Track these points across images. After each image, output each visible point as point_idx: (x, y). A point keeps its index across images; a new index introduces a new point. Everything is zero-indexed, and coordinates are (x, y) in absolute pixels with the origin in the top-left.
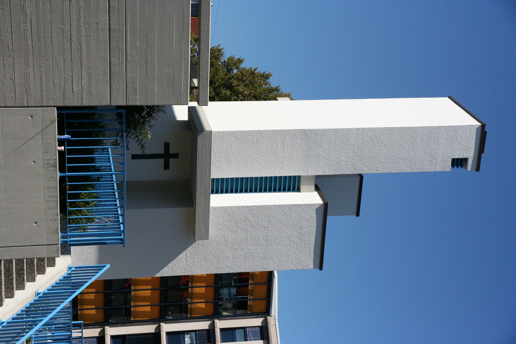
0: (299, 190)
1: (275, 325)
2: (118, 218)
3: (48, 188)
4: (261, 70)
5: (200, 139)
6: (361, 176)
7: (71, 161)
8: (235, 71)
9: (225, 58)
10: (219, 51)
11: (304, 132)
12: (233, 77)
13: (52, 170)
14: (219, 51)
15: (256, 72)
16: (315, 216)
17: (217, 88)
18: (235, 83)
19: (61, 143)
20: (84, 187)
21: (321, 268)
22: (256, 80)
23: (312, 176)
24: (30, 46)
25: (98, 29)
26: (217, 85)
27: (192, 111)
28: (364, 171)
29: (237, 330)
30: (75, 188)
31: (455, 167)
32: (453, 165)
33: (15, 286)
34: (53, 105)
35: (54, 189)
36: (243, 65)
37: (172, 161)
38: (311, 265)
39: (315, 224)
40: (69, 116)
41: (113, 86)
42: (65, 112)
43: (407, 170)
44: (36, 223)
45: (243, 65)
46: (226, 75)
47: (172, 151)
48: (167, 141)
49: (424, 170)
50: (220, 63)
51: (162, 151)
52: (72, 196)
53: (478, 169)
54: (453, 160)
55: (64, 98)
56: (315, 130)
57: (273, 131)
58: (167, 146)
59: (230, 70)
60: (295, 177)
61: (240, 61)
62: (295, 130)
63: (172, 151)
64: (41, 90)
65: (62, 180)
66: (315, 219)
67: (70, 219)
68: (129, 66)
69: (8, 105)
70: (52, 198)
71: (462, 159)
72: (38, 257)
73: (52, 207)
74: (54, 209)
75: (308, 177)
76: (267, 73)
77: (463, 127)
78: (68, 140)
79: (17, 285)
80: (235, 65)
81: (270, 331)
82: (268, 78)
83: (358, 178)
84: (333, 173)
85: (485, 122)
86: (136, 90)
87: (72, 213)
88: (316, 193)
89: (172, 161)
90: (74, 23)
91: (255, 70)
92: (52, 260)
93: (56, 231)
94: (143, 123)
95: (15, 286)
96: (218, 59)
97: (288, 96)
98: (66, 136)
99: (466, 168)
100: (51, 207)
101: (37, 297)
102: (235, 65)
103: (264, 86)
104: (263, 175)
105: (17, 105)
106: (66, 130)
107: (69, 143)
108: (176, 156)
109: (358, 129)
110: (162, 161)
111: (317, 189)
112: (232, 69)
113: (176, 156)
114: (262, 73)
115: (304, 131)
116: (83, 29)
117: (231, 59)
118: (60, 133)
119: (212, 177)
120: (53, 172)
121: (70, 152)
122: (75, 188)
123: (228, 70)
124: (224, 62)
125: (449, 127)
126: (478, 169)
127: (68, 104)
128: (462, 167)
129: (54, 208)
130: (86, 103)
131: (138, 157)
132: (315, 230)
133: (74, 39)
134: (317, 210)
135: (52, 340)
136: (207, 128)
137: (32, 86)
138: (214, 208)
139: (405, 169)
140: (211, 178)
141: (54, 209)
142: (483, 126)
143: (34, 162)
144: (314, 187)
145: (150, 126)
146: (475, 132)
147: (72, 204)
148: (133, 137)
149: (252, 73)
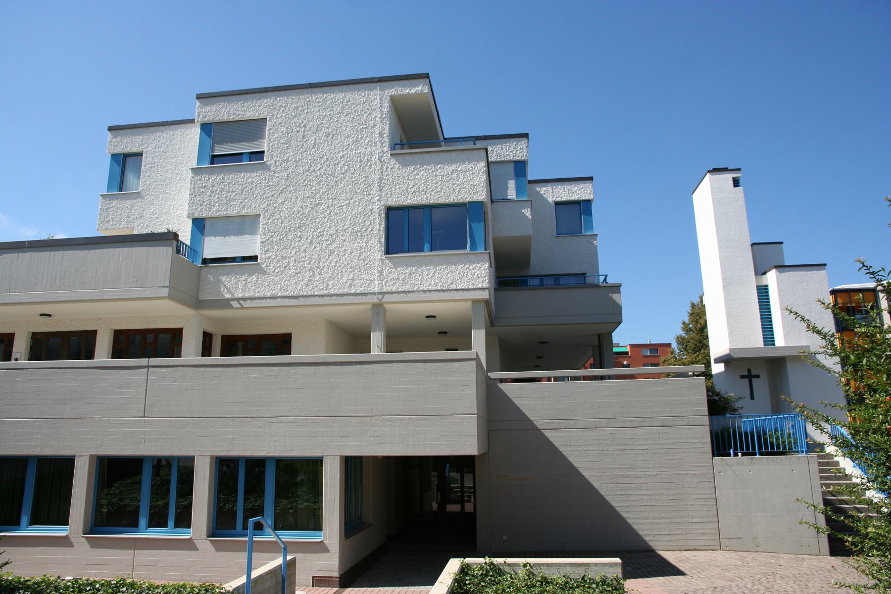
0: (767, 286)
2: (785, 417)
4: (689, 309)
5: (735, 356)
6: (753, 245)
7: (748, 448)
8: (691, 326)
9: (683, 334)
10: (678, 338)
11: (725, 286)
12: (695, 327)
14: (678, 338)
15: (690, 312)
16: (785, 273)
17: (703, 337)
18: (699, 326)
19: (736, 455)
20: (766, 440)
21: (825, 265)
22: (696, 312)
23: (756, 278)
24: (676, 472)
25: (662, 433)
26: (701, 338)
27: (717, 361)
28: (748, 243)
30: (766, 446)
31: (740, 184)
32: (738, 186)
33: (848, 482)
34: (711, 460)
36: (687, 321)
37: (753, 373)
38: (823, 272)
39: (791, 273)
40: (718, 449)
41: (697, 423)
42: (715, 452)
43: (745, 215)
44: (793, 471)
45: (687, 321)
46: (694, 332)
47: (746, 373)
48: (739, 377)
49: (744, 204)
50: (687, 336)
51: (747, 380)
52: (772, 448)
53: (740, 170)
54: (735, 186)
55: (707, 453)
56: (723, 280)
57: (726, 307)
58: (743, 377)
59: (691, 330)
60: (757, 289)
61: (684, 323)
62: (724, 293)
63: (746, 373)
64: (703, 466)
65: (761, 454)
66: (788, 273)
67: (789, 449)
68: (682, 414)
69: (714, 486)
71: (734, 181)
72: (818, 472)
75: (757, 281)
76: (690, 305)
77: (711, 184)
78: (734, 450)
79: (849, 480)
80: (687, 327)
82: (694, 304)
83: (755, 246)
84: (752, 264)
85: (706, 171)
86: (698, 410)
87: (784, 448)
88: (768, 274)
89: (753, 373)
90: (660, 447)
91: (689, 313)
94: (724, 398)
95: (848, 482)
96: (684, 338)
97: (701, 298)
98: (731, 451)
99: (739, 177)
101: (857, 467)
102: (687, 327)
103: (700, 306)
104: (758, 311)
105: (713, 480)
106: (727, 452)
107: (736, 449)
108: (749, 371)
109: (719, 252)
110: (754, 380)
111: (764, 273)
112: (690, 328)
113: (749, 371)
114: (691, 308)
115: (724, 287)
116: (663, 442)
117: (683, 329)
118: (729, 455)
119: (762, 346)
121: (742, 449)
122: (766, 446)
123: (691, 331)
124: (685, 333)
125: (712, 193)
126: (740, 170)
127: (710, 450)
128: (739, 180)
130: (709, 440)
132: (796, 272)
133: (669, 447)
134: (781, 272)
136: (727, 352)
137: (701, 472)
138: (785, 343)
139: (744, 217)
140: (763, 346)
142: (709, 171)
143: (750, 471)
144: (764, 276)
145: (726, 394)
146: (713, 176)
147: (778, 447)
148: (734, 404)
149: (692, 314)
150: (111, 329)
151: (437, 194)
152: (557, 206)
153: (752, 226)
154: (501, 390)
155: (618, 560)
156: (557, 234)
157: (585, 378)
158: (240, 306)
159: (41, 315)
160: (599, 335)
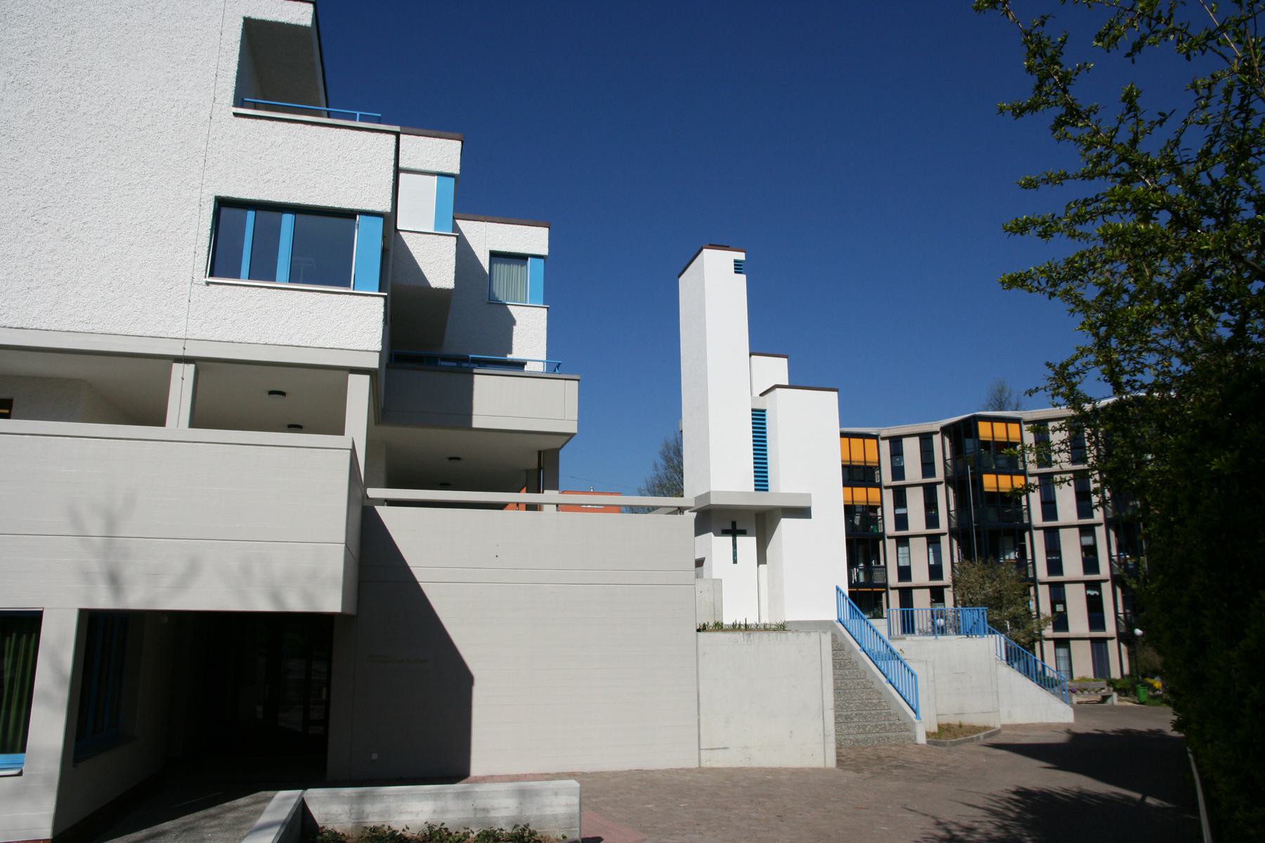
37: (739, 527)
47: (729, 527)
63: (729, 527)
89: (739, 527)
108: (734, 524)
113: (734, 524)
150: (809, 496)
151: (309, 190)
152: (493, 258)
153: (842, 423)
154: (375, 510)
155: (875, 582)
156: (489, 300)
157: (633, 509)
158: (568, 437)
159: (271, 393)
160: (540, 453)
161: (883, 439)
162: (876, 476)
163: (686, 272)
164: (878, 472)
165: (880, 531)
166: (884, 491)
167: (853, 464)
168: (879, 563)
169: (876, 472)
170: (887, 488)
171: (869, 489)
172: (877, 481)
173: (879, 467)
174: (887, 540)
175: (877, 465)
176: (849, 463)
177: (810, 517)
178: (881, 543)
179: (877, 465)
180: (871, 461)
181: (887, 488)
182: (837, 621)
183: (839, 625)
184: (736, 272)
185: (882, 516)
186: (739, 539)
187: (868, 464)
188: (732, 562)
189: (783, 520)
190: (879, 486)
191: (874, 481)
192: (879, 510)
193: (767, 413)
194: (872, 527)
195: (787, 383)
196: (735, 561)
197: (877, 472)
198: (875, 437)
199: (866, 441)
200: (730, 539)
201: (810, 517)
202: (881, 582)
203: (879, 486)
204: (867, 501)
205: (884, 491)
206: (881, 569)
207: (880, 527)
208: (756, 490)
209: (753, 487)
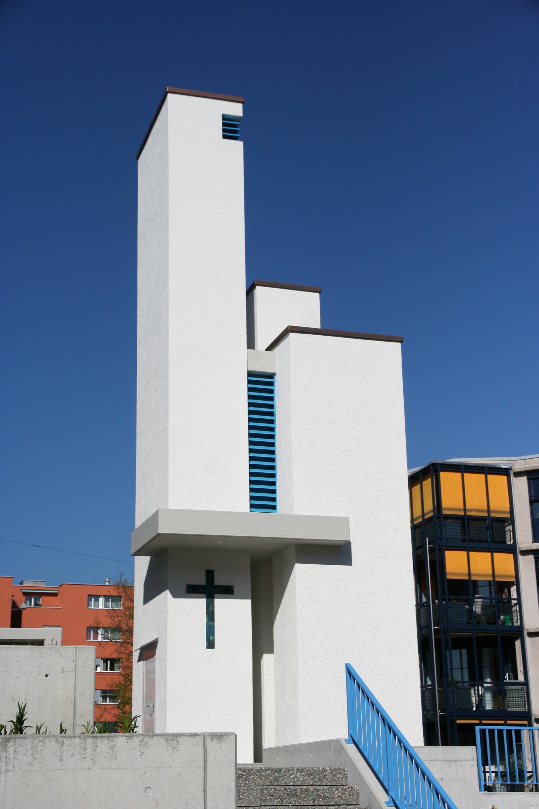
1: (525, 459)
3: (61, 760)
13: (15, 751)
29: (535, 518)
35: (64, 745)
37: (219, 581)
47: (201, 581)
63: (201, 581)
70: (87, 751)
73: (110, 752)
74: (115, 745)
81: (535, 467)
89: (219, 581)
92: (334, 775)
93: (170, 742)
100: (109, 753)
108: (210, 574)
113: (210, 574)
120: (20, 749)
129: (112, 747)
131: (211, 638)
135: (91, 601)
141: (115, 745)
155: (509, 709)
161: (518, 474)
162: (508, 534)
163: (147, 146)
164: (510, 528)
165: (515, 624)
166: (521, 559)
167: (468, 513)
168: (516, 678)
169: (507, 528)
170: (525, 553)
171: (496, 555)
172: (510, 542)
173: (511, 521)
174: (527, 639)
175: (508, 516)
176: (462, 513)
177: (348, 562)
178: (518, 643)
179: (508, 516)
180: (499, 509)
181: (525, 553)
182: (347, 741)
183: (351, 749)
184: (225, 137)
185: (519, 599)
186: (220, 603)
187: (492, 515)
188: (204, 644)
189: (296, 564)
190: (512, 550)
191: (505, 542)
192: (513, 589)
193: (277, 380)
194: (502, 617)
195: (317, 325)
196: (210, 644)
197: (509, 528)
198: (505, 472)
199: (490, 477)
200: (201, 603)
201: (348, 562)
202: (521, 709)
203: (512, 550)
204: (494, 575)
205: (521, 559)
206: (519, 687)
207: (516, 617)
208: (252, 506)
209: (247, 502)
